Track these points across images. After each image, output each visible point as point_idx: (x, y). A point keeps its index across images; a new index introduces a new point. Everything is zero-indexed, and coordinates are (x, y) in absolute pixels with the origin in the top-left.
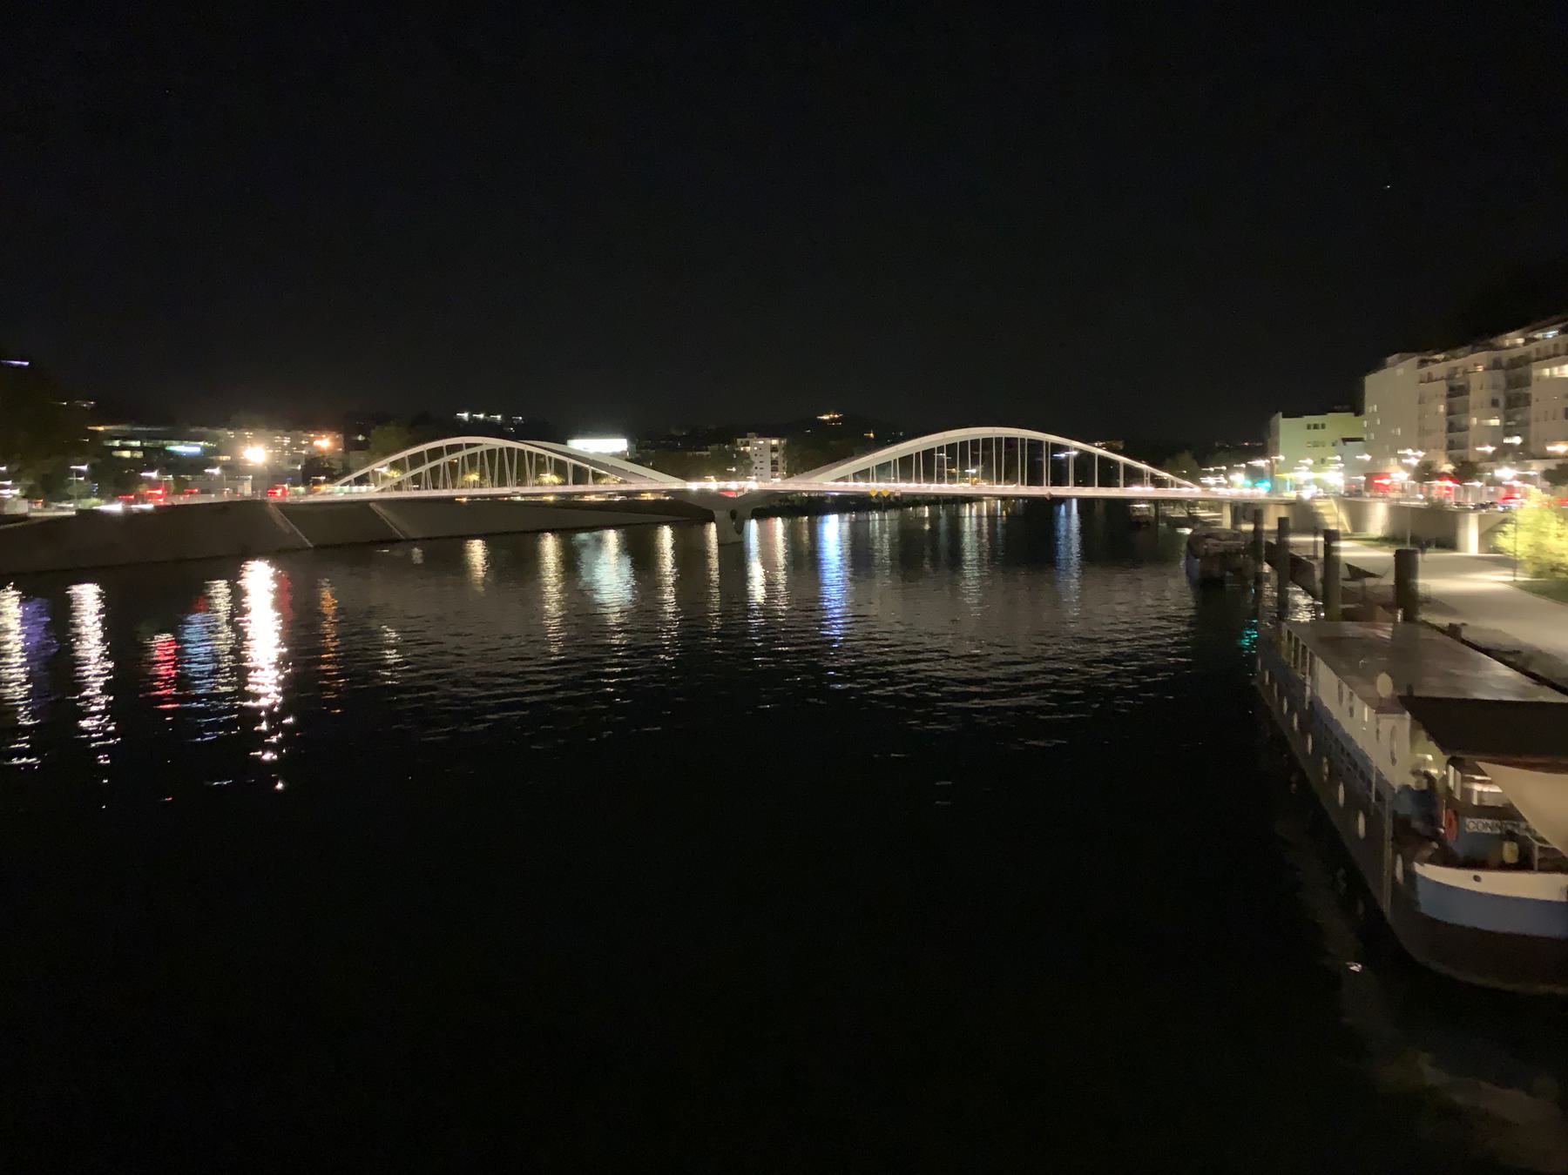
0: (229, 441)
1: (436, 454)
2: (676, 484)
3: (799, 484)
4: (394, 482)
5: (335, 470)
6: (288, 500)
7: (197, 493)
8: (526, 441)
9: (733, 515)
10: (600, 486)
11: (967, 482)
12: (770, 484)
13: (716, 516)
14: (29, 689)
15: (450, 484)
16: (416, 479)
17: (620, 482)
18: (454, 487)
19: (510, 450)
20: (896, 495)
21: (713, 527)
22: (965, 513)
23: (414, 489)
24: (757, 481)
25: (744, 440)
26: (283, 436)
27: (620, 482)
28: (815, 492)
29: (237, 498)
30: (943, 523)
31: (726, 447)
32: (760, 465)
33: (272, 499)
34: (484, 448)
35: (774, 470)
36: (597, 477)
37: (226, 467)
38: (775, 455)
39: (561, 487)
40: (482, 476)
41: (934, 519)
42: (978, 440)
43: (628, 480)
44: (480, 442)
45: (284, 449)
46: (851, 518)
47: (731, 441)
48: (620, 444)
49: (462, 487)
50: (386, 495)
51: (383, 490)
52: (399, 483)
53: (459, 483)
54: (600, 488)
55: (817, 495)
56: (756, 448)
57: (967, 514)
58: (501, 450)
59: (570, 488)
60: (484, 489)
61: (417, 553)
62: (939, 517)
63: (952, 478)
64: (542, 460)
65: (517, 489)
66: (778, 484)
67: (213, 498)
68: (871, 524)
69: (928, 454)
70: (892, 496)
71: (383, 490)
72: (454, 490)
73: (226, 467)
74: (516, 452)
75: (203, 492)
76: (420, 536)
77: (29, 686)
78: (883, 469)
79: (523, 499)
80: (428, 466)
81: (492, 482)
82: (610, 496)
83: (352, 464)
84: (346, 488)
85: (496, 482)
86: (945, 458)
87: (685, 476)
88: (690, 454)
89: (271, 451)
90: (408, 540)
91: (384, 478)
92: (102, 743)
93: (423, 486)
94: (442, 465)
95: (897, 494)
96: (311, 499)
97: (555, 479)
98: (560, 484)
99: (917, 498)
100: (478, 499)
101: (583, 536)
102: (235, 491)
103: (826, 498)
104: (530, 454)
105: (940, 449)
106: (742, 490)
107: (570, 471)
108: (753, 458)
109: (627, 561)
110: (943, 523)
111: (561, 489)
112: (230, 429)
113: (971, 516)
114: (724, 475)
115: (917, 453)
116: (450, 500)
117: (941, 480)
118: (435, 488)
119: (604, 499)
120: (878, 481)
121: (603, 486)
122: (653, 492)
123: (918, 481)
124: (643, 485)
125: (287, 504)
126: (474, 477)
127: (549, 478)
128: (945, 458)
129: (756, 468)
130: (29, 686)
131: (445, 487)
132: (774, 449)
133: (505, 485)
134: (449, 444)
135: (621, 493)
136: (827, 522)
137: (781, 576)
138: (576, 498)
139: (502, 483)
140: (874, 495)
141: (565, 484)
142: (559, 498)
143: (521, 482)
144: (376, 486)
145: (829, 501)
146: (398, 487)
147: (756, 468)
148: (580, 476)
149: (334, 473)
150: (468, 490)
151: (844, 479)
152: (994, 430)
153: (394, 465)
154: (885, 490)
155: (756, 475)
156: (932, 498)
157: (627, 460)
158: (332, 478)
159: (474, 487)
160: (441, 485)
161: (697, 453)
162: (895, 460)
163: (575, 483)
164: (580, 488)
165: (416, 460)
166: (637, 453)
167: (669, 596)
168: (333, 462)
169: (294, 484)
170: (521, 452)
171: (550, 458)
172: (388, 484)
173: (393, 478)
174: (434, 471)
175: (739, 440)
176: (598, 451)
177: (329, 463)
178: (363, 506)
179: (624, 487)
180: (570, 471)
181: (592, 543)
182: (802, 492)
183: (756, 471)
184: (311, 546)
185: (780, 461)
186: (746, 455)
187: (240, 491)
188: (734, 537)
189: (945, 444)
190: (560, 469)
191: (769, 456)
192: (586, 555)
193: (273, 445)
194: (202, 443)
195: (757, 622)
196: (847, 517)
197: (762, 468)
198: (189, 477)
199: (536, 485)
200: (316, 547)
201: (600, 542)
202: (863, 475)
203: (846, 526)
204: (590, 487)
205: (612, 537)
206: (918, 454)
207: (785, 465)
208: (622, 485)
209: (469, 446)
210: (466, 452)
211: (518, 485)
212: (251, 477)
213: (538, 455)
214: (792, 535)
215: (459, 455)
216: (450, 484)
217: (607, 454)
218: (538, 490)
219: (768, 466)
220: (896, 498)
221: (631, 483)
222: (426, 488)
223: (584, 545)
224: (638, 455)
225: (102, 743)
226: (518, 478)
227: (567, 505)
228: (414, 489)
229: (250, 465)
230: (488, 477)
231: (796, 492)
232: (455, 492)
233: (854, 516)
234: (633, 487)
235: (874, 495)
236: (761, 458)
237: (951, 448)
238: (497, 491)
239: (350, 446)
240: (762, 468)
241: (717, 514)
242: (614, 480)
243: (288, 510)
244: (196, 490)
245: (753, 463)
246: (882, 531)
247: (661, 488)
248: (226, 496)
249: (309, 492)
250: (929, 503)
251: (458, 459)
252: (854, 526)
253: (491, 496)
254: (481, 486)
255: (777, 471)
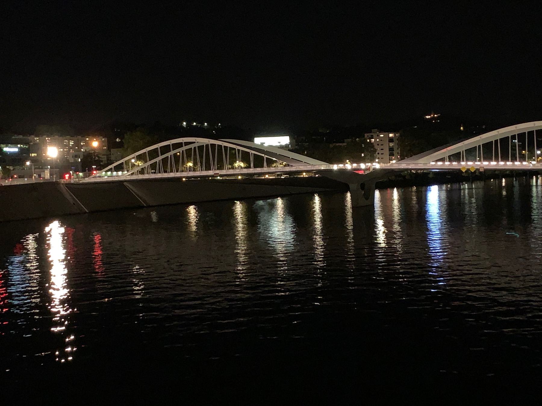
0: (36, 144)
1: (166, 149)
2: (323, 166)
3: (409, 164)
4: (139, 169)
5: (102, 161)
6: (72, 182)
7: (16, 178)
8: (222, 140)
9: (363, 186)
10: (272, 168)
11: (534, 160)
12: (389, 165)
13: (350, 187)
14: (401, 221)
15: (174, 169)
16: (153, 166)
17: (285, 166)
18: (177, 171)
19: (213, 145)
20: (481, 170)
21: (349, 195)
22: (532, 183)
23: (152, 173)
24: (378, 163)
25: (369, 134)
26: (69, 140)
27: (285, 166)
28: (421, 169)
29: (41, 181)
30: (516, 189)
31: (357, 139)
32: (382, 152)
33: (62, 181)
34: (196, 145)
35: (391, 154)
36: (270, 163)
37: (33, 160)
38: (391, 145)
39: (245, 170)
40: (195, 164)
41: (509, 187)
42: (533, 131)
43: (290, 164)
44: (194, 141)
45: (71, 148)
46: (447, 187)
47: (361, 136)
48: (285, 140)
49: (182, 171)
50: (134, 177)
51: (132, 174)
52: (142, 169)
53: (180, 169)
54: (272, 169)
55: (422, 171)
56: (378, 140)
57: (534, 184)
58: (207, 146)
59: (252, 170)
60: (197, 172)
61: (154, 215)
62: (513, 186)
63: (523, 158)
64: (234, 152)
65: (217, 172)
66: (394, 164)
67: (26, 181)
68: (462, 191)
69: (504, 141)
70: (477, 171)
71: (132, 174)
72: (177, 173)
73: (33, 160)
74: (217, 146)
75: (20, 177)
76: (155, 204)
77: (401, 220)
78: (471, 154)
79: (221, 179)
80: (161, 158)
81: (202, 167)
82: (278, 175)
83: (113, 158)
84: (109, 173)
85: (204, 168)
86: (517, 143)
87: (331, 161)
88: (331, 146)
89: (62, 150)
90: (149, 206)
91: (133, 165)
92: (534, 332)
93: (157, 171)
94: (158, 162)
95: (481, 170)
96: (87, 180)
97: (242, 165)
98: (245, 168)
99: (497, 172)
100: (192, 179)
101: (261, 203)
102: (40, 176)
103: (429, 174)
104: (226, 147)
105: (513, 137)
106: (369, 169)
107: (252, 159)
108: (376, 147)
109: (290, 220)
110: (516, 189)
111: (245, 171)
112: (36, 136)
113: (537, 185)
114: (357, 159)
115: (495, 141)
116: (179, 179)
117: (514, 159)
118: (165, 172)
119: (274, 177)
120: (467, 160)
121: (274, 168)
122: (307, 172)
123: (497, 160)
124: (301, 167)
125: (72, 184)
126: (190, 164)
127: (239, 164)
128: (517, 143)
129: (378, 154)
130: (401, 220)
131: (171, 171)
132: (391, 140)
133: (210, 169)
134: (115, 165)
135: (286, 173)
136: (430, 191)
137: (396, 227)
138: (256, 177)
139: (208, 168)
140: (464, 171)
141: (249, 167)
142: (244, 177)
143: (220, 168)
144: (128, 171)
145: (431, 176)
146: (142, 172)
147: (378, 154)
148: (259, 162)
149: (101, 163)
150: (186, 173)
151: (442, 160)
152: (447, 149)
153: (139, 158)
154: (473, 167)
155: (378, 158)
156: (508, 172)
157: (290, 150)
158: (100, 168)
159: (190, 171)
160: (169, 170)
161: (337, 144)
162: (479, 146)
163: (255, 167)
164: (259, 170)
165: (153, 154)
166: (296, 145)
167: (319, 240)
168: (101, 156)
169: (76, 171)
170: (220, 146)
171: (239, 150)
172: (135, 170)
173: (138, 166)
174: (165, 161)
175: (366, 135)
176: (271, 144)
177: (98, 157)
178: (120, 183)
179: (288, 169)
180: (252, 159)
181: (267, 207)
182: (411, 170)
183: (378, 156)
184: (87, 211)
185: (395, 149)
186: (371, 145)
187: (42, 176)
188: (363, 202)
189: (498, 139)
190: (245, 157)
191: (387, 146)
192: (262, 216)
193: (63, 147)
194: (19, 146)
195: (381, 259)
196: (444, 187)
197: (382, 154)
198: (11, 168)
199: (230, 169)
200: (92, 212)
201: (273, 206)
202: (456, 157)
203: (444, 194)
204: (265, 169)
205: (280, 202)
206: (496, 141)
207: (399, 151)
208: (286, 168)
209: (187, 144)
210: (184, 148)
211: (218, 169)
212: (49, 167)
213: (232, 149)
214: (404, 200)
215: (180, 150)
216: (174, 169)
217: (276, 147)
218: (231, 172)
219: (387, 152)
220: (480, 173)
221: (292, 166)
222: (160, 172)
223: (262, 208)
224: (296, 147)
225: (534, 332)
226: (218, 164)
227: (249, 180)
228: (152, 173)
229: (48, 159)
230: (199, 164)
231: (407, 170)
232: (178, 175)
233: (449, 186)
234: (293, 169)
235: (464, 171)
236: (382, 147)
237: (521, 136)
238: (205, 173)
239: (111, 145)
240: (382, 154)
241: (351, 186)
242: (281, 164)
243: (71, 187)
244: (15, 176)
245: (375, 151)
246: (471, 196)
247: (313, 169)
248: (34, 179)
249: (85, 177)
250: (505, 176)
251: (179, 152)
252: (449, 193)
253: (201, 177)
254: (194, 170)
255: (393, 155)
